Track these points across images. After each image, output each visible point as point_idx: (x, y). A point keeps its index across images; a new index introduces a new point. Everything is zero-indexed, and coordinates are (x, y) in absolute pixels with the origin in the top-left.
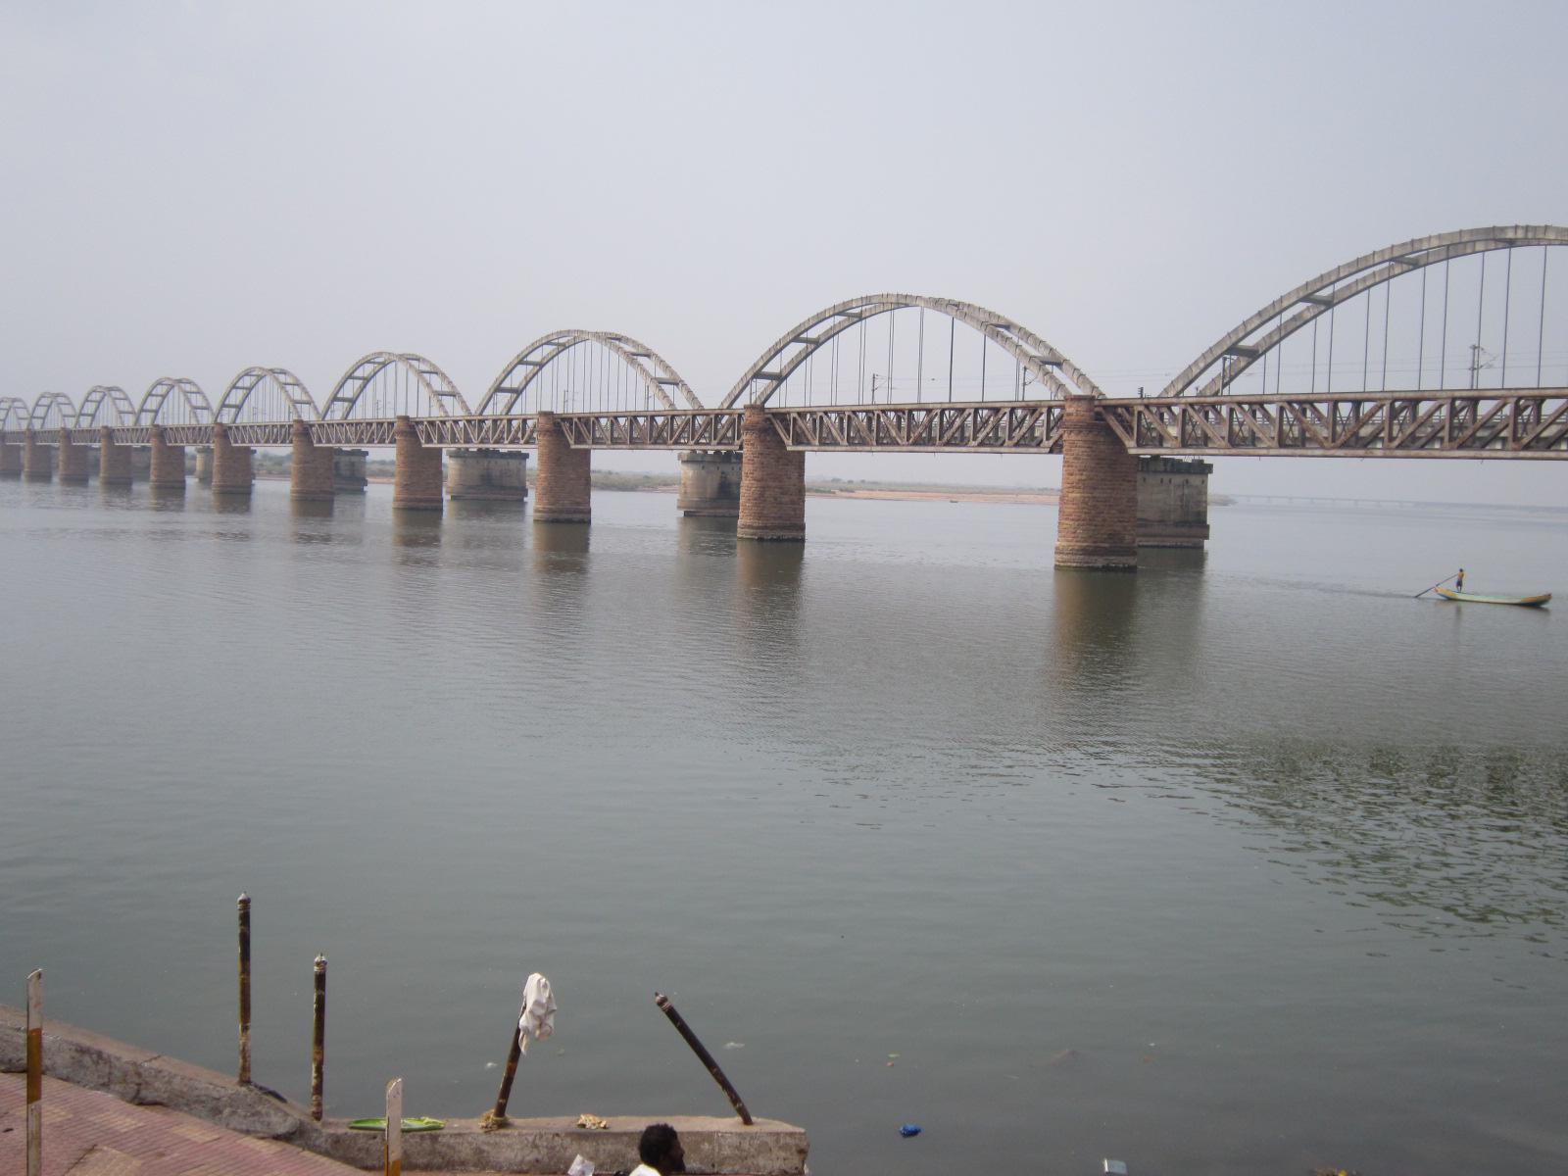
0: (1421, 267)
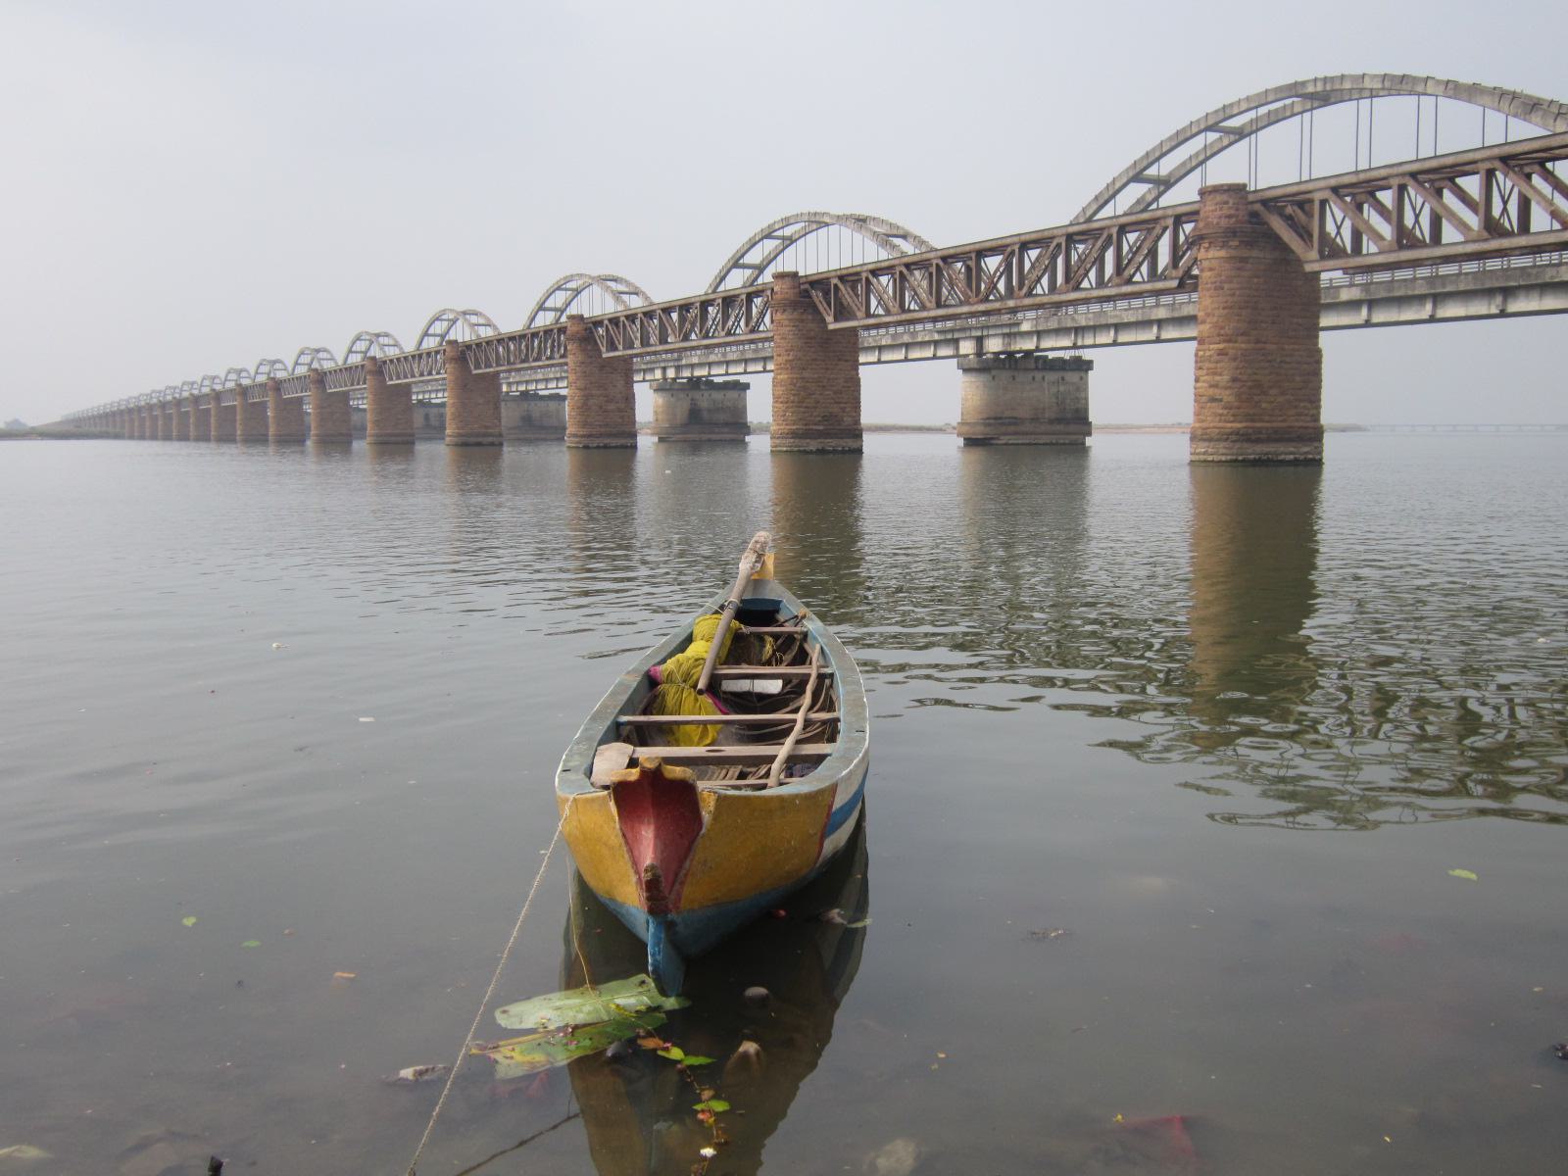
0: (1245, 136)
